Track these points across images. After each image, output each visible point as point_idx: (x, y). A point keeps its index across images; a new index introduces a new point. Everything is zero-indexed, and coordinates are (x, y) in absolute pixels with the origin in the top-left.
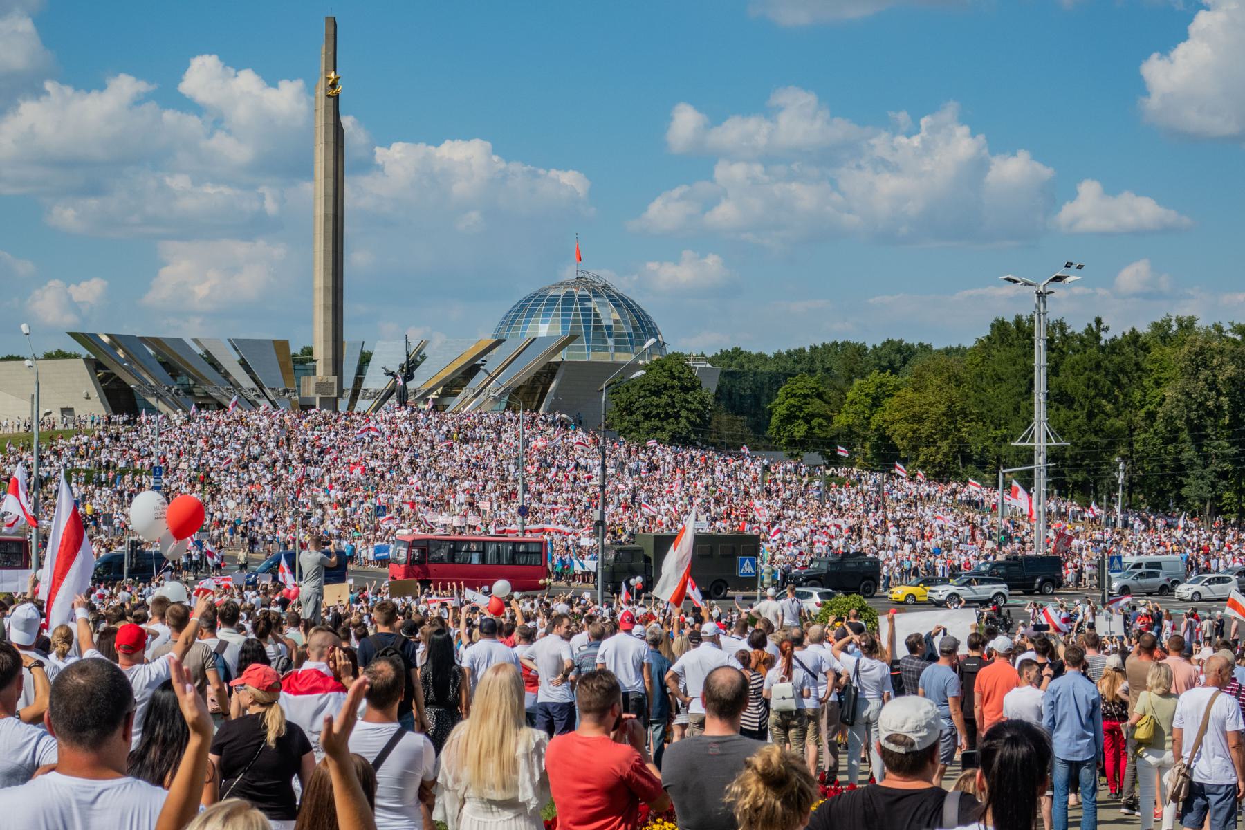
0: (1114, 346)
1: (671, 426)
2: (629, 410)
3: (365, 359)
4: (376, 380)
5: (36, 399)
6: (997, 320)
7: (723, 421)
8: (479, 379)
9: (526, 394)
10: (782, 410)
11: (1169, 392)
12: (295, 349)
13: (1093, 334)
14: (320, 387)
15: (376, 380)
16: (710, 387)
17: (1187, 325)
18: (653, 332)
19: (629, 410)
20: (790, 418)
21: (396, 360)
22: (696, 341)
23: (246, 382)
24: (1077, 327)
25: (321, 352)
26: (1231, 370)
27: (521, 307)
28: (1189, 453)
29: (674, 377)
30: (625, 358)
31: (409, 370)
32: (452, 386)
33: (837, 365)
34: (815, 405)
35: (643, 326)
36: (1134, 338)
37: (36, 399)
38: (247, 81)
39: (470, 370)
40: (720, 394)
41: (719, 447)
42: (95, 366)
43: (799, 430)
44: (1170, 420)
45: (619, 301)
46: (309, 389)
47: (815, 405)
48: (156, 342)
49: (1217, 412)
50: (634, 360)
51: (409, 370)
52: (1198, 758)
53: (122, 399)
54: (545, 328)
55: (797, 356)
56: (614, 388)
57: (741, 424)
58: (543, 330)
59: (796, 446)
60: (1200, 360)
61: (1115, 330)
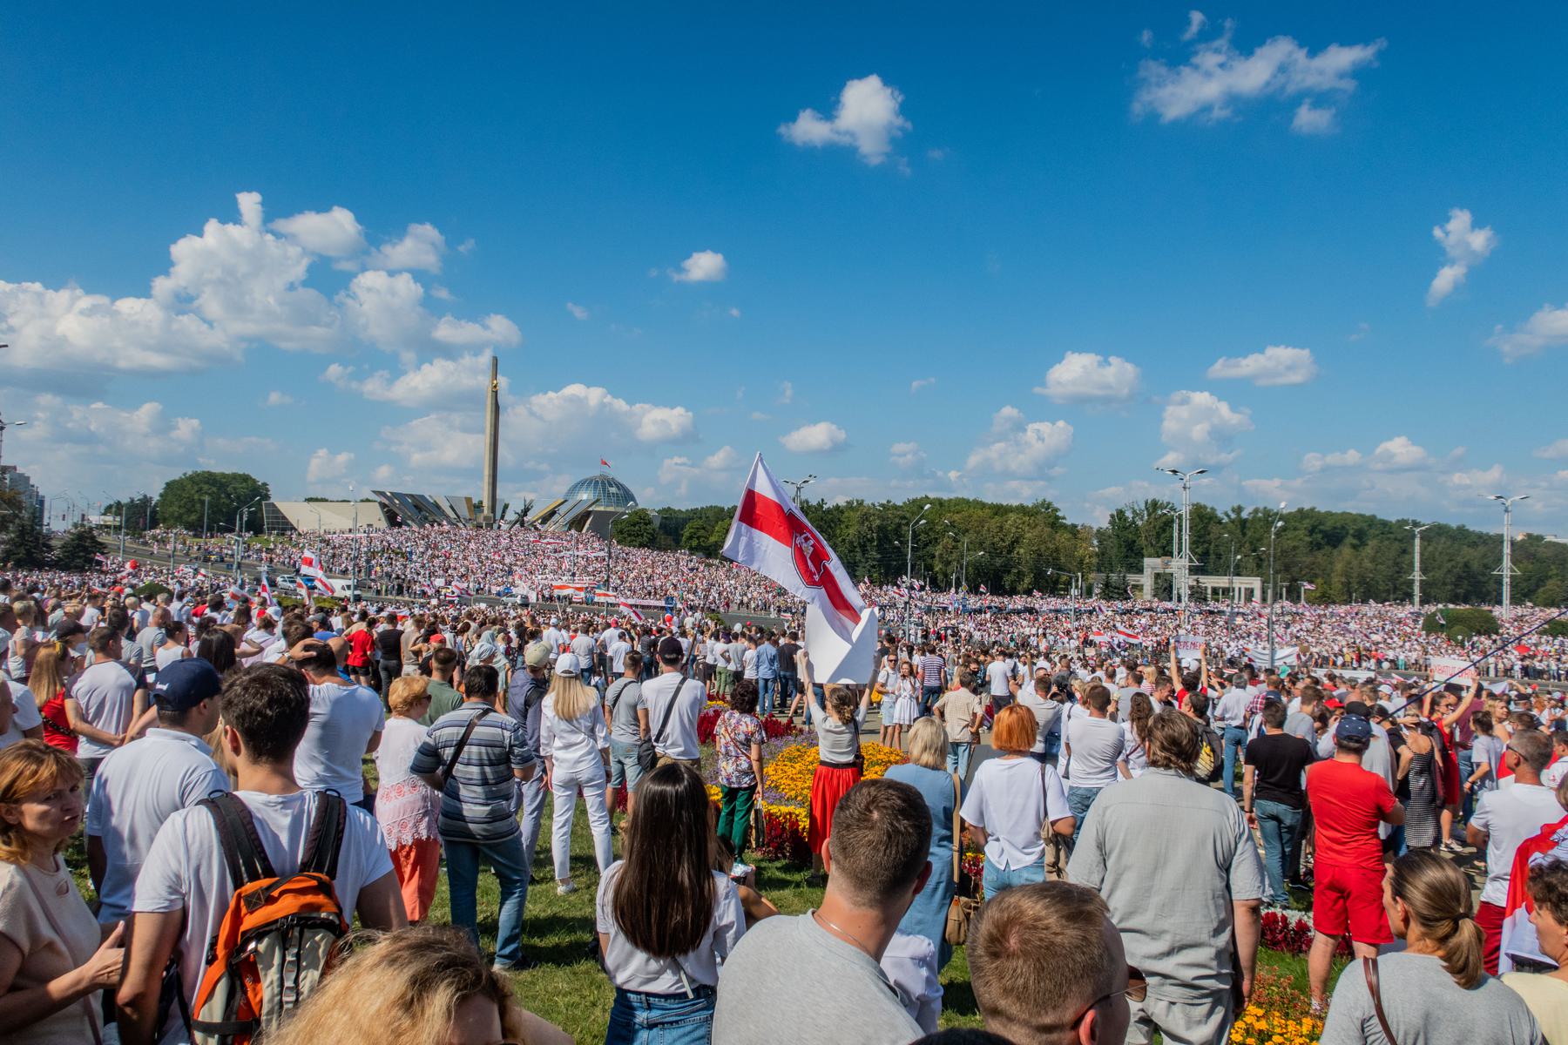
0: (829, 511)
1: (639, 540)
2: (621, 532)
3: (506, 507)
4: (511, 516)
5: (356, 520)
6: (265, 484)
7: (662, 539)
8: (556, 517)
9: (578, 523)
10: (687, 534)
11: (851, 531)
12: (475, 501)
13: (820, 505)
14: (486, 518)
15: (511, 516)
16: (657, 523)
17: (860, 503)
18: (633, 499)
19: (621, 532)
20: (691, 538)
21: (520, 508)
22: (649, 500)
23: (452, 515)
24: (814, 503)
25: (486, 504)
26: (878, 522)
27: (575, 487)
28: (859, 556)
29: (641, 518)
30: (621, 510)
31: (526, 512)
32: (545, 519)
33: (710, 514)
34: (702, 532)
35: (627, 496)
36: (837, 507)
37: (356, 520)
38: (551, 394)
39: (553, 513)
40: (662, 526)
41: (659, 549)
42: (383, 505)
43: (694, 543)
44: (851, 542)
45: (619, 486)
46: (481, 519)
47: (702, 532)
48: (412, 496)
49: (871, 541)
50: (625, 511)
51: (526, 512)
52: (273, 996)
53: (392, 519)
54: (585, 496)
55: (695, 511)
56: (615, 523)
57: (670, 541)
58: (585, 497)
59: (693, 550)
60: (865, 517)
61: (829, 505)
